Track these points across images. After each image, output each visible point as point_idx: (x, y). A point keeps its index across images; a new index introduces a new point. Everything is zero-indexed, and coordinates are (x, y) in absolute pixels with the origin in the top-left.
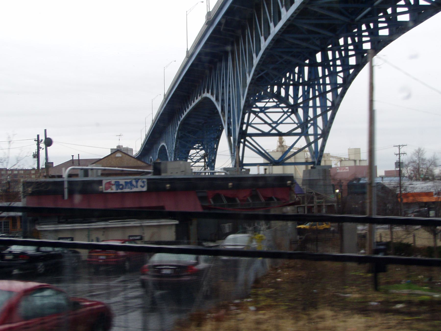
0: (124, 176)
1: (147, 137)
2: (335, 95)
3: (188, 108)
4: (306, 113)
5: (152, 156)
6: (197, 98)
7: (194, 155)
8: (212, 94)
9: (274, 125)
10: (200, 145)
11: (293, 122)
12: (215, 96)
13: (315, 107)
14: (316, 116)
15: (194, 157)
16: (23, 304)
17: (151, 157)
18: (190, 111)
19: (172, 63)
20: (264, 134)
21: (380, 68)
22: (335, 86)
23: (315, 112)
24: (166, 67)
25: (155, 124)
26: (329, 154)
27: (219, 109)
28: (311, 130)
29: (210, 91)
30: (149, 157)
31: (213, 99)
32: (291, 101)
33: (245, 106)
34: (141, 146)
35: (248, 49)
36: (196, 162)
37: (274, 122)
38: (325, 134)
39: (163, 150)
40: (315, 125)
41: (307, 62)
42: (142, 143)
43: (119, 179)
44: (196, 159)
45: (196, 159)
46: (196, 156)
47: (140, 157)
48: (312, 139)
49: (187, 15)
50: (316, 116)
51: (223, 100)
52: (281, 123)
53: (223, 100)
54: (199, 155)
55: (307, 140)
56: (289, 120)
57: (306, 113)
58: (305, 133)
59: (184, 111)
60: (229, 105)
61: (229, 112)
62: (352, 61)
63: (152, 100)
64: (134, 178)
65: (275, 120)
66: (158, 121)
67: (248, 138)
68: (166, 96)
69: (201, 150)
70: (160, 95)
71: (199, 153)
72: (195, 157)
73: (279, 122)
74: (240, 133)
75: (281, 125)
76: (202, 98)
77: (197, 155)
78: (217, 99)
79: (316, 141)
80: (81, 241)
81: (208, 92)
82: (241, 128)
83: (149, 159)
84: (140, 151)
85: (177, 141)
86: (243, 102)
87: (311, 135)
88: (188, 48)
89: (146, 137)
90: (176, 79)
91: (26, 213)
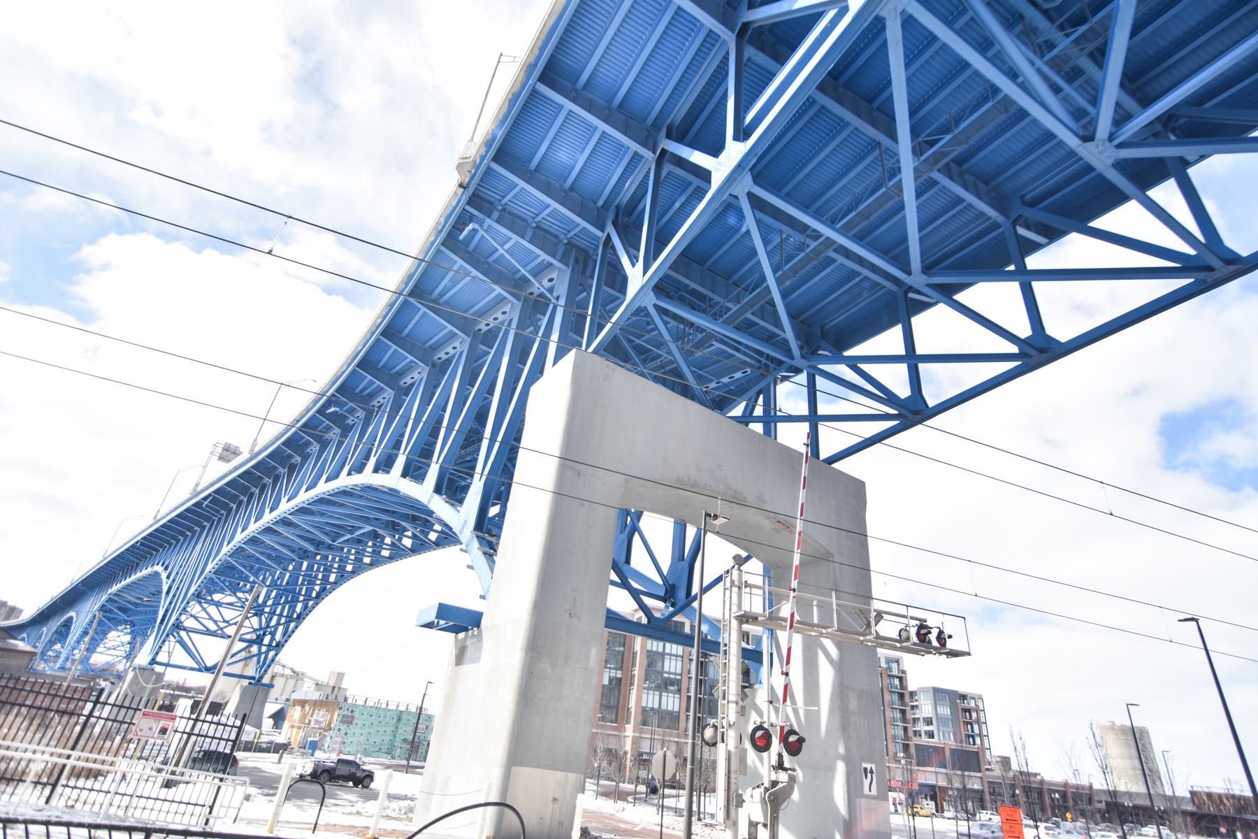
2: (306, 607)
4: (269, 621)
9: (222, 625)
14: (278, 624)
16: (1081, 134)
17: (45, 629)
20: (209, 633)
21: (1137, 392)
22: (308, 596)
23: (279, 620)
27: (165, 588)
28: (267, 640)
30: (42, 627)
35: (850, 220)
36: (109, 649)
37: (225, 621)
38: (279, 646)
39: (70, 620)
40: (273, 634)
46: (211, 618)
48: (264, 649)
55: (260, 649)
57: (269, 621)
58: (259, 641)
61: (174, 596)
62: (332, 578)
65: (227, 618)
67: (183, 633)
70: (315, 381)
73: (231, 622)
78: (168, 577)
79: (267, 653)
80: (1231, 96)
83: (40, 630)
85: (53, 634)
86: (192, 590)
87: (265, 645)
91: (579, 775)
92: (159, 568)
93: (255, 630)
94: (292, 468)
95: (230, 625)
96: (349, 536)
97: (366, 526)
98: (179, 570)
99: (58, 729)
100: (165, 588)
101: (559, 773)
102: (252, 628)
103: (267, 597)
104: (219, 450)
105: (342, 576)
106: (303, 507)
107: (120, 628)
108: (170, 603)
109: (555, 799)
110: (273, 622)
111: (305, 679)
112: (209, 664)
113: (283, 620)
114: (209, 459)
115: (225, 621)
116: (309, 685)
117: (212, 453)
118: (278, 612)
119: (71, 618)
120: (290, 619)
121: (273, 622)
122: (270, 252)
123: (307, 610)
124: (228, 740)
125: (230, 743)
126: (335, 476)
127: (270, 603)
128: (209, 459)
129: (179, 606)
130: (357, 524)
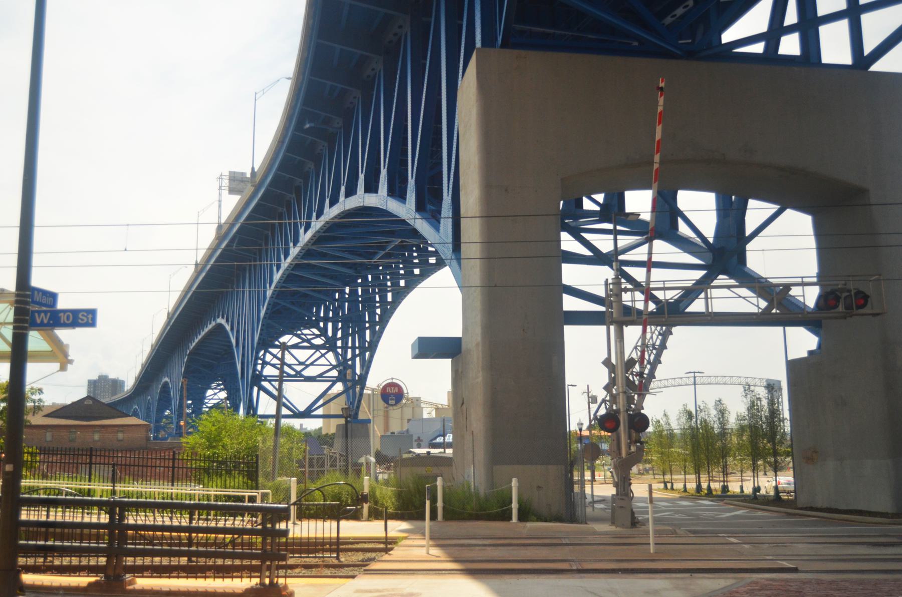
0: (74, 420)
1: (154, 350)
2: (373, 333)
3: (200, 334)
5: (150, 396)
6: (210, 323)
7: (210, 397)
8: (227, 321)
9: (298, 368)
10: (221, 382)
11: (329, 364)
12: (230, 323)
13: (353, 348)
14: (354, 356)
15: (210, 399)
18: (202, 338)
19: (279, 82)
22: (373, 323)
24: (262, 93)
25: (155, 351)
26: (420, 398)
27: (233, 341)
29: (225, 316)
31: (228, 328)
32: (330, 333)
33: (258, 343)
34: (151, 349)
37: (301, 363)
39: (166, 388)
41: (359, 281)
42: (153, 343)
43: (447, 191)
44: (731, 291)
45: (731, 291)
46: (212, 399)
47: (133, 395)
49: (256, 100)
50: (353, 358)
51: (238, 331)
52: (312, 364)
53: (238, 331)
54: (218, 398)
56: (322, 361)
59: (195, 337)
60: (244, 339)
61: (244, 347)
63: (170, 275)
64: (799, 574)
65: (302, 360)
66: (159, 347)
68: (170, 316)
69: (221, 390)
71: (218, 394)
72: (211, 400)
74: (253, 377)
75: (311, 367)
76: (216, 324)
77: (214, 398)
78: (232, 329)
81: (371, 188)
82: (255, 370)
84: (134, 386)
88: (255, 166)
89: (153, 350)
90: (269, 161)
92: (222, 321)
93: (334, 367)
94: (298, 191)
95: (307, 366)
96: (382, 253)
97: (393, 239)
98: (239, 319)
99: (218, 482)
100: (233, 341)
101: (539, 467)
102: (331, 365)
103: (335, 330)
104: (226, 182)
105: (398, 293)
106: (320, 236)
107: (213, 385)
108: (243, 355)
109: (539, 487)
110: (349, 356)
111: (422, 405)
112: (302, 408)
113: (357, 352)
114: (220, 195)
115: (301, 363)
116: (428, 410)
117: (220, 188)
118: (350, 345)
119: (166, 385)
120: (363, 350)
121: (349, 356)
122: (126, 250)
123: (377, 337)
124: (169, 459)
125: (171, 461)
126: (320, 214)
127: (339, 334)
128: (220, 195)
129: (251, 358)
130: (388, 239)
